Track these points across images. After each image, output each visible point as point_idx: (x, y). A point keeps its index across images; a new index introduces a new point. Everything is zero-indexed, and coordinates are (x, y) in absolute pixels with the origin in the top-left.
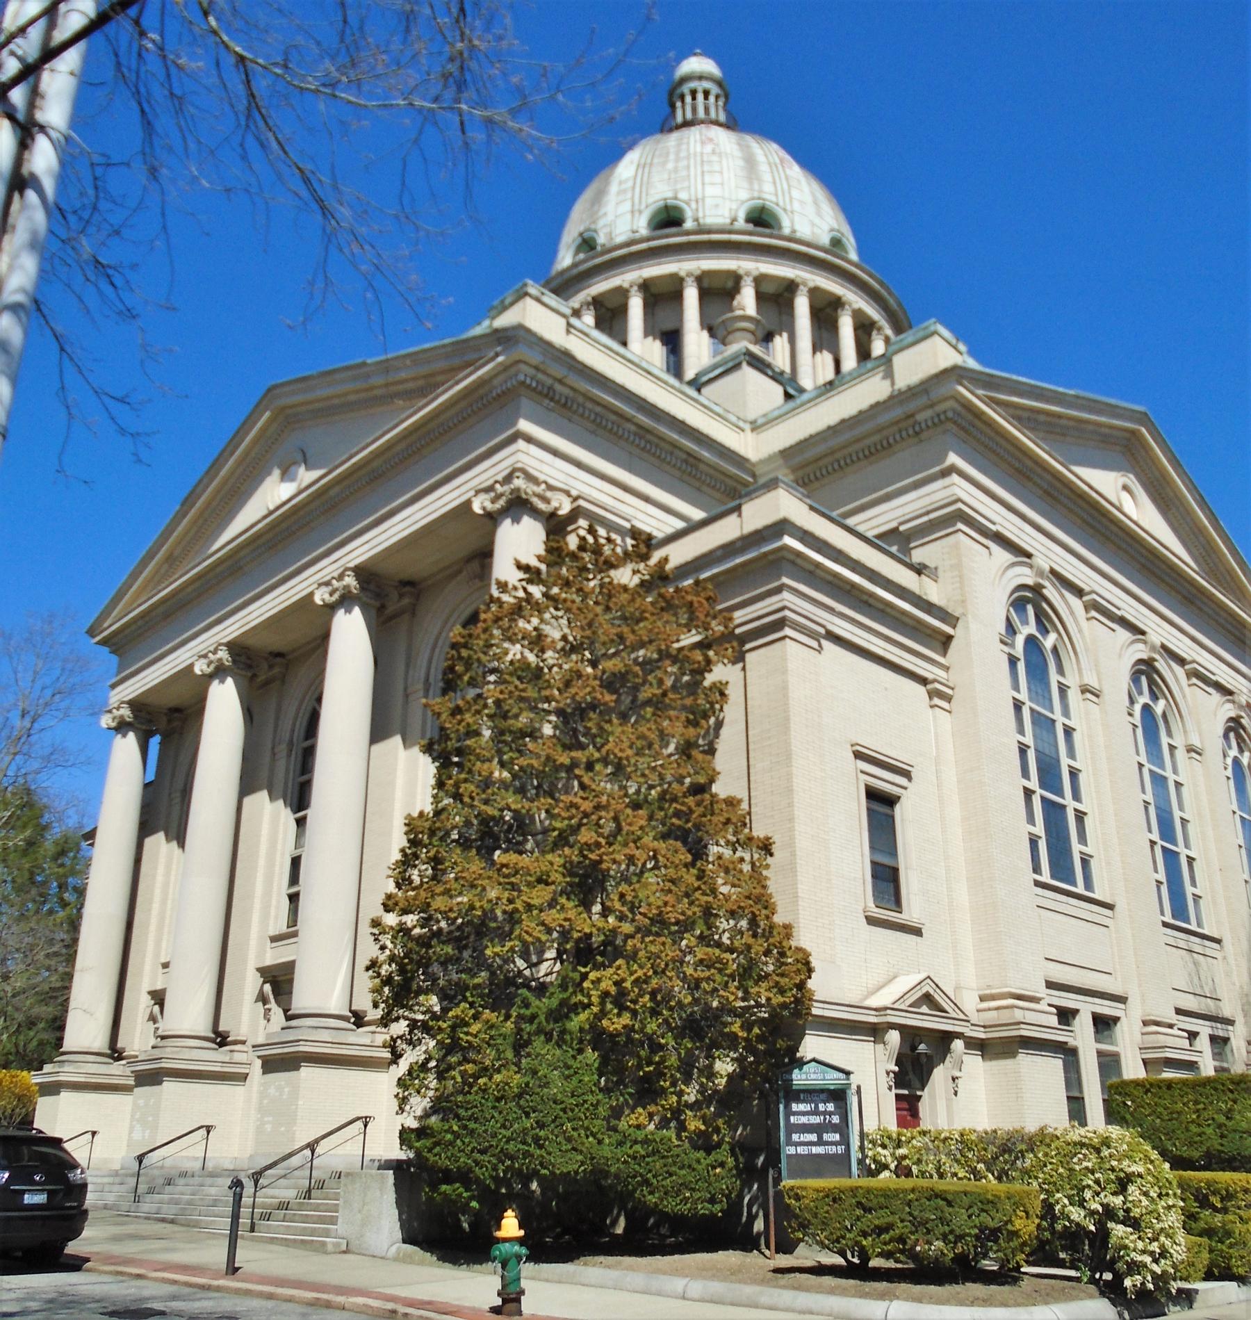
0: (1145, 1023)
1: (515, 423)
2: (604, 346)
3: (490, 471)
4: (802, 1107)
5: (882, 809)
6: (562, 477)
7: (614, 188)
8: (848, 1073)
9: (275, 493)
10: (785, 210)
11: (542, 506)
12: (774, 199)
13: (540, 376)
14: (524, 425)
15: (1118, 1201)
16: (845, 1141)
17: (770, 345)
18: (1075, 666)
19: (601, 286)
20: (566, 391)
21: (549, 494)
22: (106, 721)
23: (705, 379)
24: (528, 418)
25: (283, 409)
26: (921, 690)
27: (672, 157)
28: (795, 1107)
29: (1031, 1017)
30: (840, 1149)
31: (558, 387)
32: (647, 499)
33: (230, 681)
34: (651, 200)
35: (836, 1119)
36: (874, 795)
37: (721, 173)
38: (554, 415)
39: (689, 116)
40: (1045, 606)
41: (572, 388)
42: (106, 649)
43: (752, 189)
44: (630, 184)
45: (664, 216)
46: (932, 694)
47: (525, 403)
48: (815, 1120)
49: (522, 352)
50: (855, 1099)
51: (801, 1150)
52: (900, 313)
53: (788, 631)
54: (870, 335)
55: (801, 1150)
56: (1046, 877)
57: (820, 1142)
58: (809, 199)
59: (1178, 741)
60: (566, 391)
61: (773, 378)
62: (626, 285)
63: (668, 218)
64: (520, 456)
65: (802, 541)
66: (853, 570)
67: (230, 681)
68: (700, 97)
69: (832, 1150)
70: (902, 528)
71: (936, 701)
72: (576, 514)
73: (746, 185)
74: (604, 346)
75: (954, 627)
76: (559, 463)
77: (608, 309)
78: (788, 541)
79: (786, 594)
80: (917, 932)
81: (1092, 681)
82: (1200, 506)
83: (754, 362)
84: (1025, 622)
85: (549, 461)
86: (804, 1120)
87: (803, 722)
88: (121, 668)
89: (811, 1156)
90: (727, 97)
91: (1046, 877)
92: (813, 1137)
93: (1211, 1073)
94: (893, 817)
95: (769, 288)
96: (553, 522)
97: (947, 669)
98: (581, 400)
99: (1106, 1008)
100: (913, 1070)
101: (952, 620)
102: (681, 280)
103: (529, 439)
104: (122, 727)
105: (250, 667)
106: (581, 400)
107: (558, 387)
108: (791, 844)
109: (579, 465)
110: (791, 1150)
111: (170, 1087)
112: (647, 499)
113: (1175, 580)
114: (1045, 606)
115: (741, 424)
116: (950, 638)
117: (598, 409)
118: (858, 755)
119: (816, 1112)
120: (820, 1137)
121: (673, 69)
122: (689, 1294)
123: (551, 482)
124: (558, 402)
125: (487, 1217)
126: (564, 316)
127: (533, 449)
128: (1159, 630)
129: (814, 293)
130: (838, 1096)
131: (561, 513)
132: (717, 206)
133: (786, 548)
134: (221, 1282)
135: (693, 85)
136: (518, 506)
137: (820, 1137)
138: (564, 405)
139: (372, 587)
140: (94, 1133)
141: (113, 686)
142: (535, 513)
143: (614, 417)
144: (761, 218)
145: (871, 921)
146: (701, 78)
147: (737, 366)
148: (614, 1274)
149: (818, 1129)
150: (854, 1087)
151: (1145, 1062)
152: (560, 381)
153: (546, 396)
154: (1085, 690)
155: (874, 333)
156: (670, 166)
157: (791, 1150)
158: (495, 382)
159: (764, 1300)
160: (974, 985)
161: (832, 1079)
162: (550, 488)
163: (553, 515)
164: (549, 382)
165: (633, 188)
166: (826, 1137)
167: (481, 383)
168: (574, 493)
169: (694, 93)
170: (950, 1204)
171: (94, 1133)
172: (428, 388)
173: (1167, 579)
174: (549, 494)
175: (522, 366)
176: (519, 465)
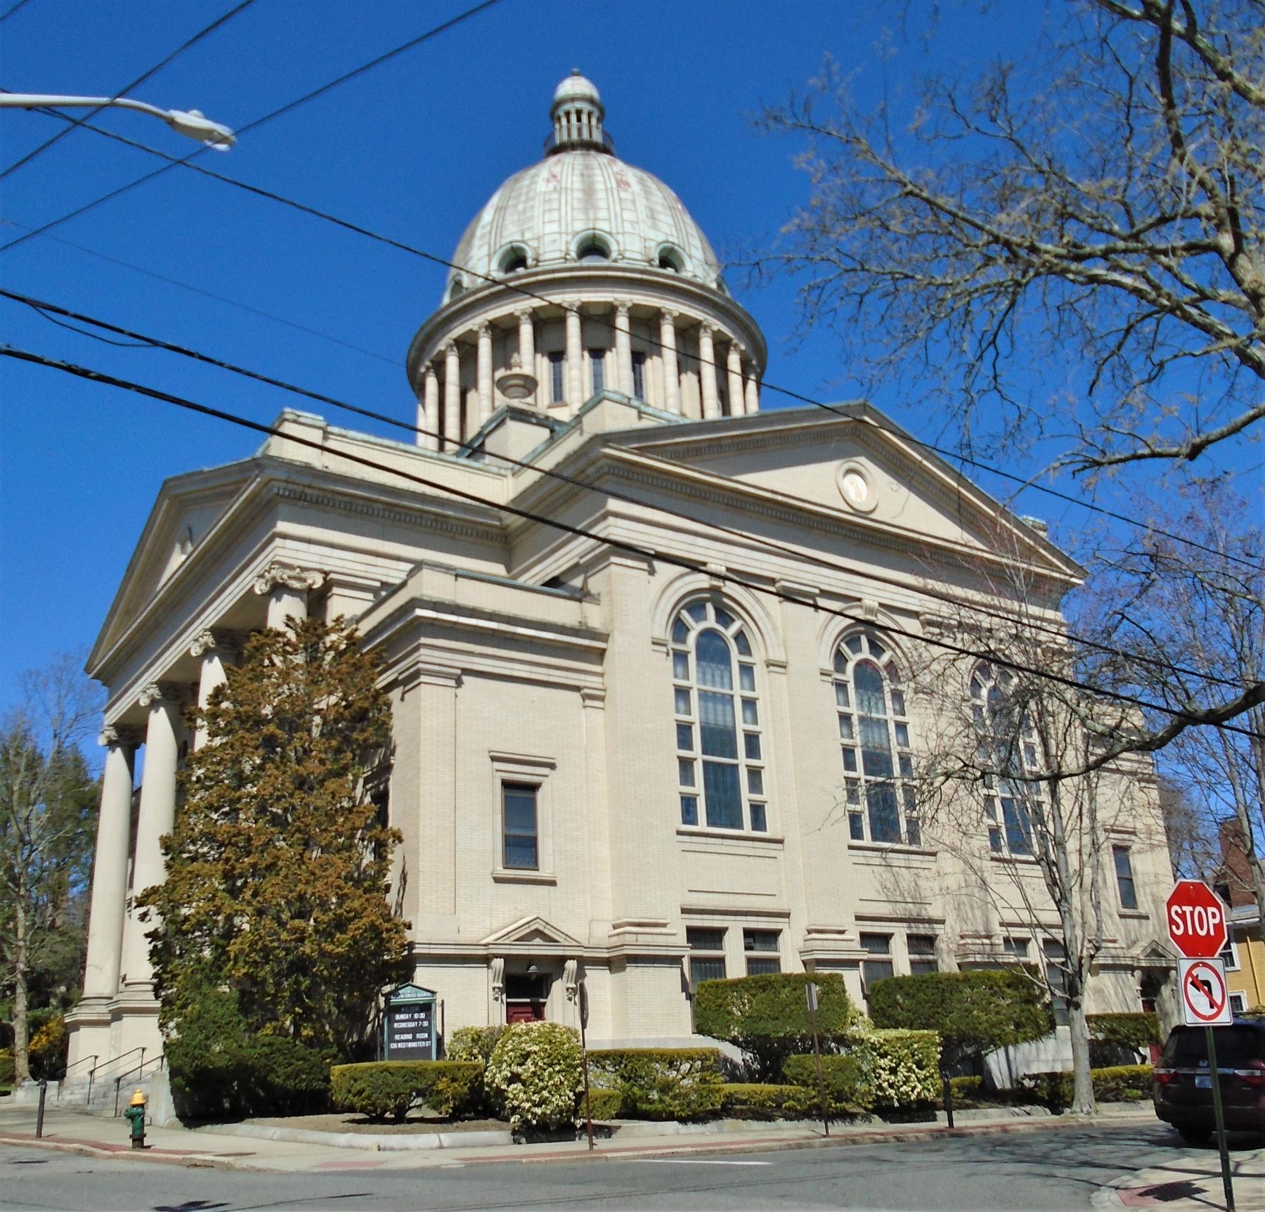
0: (809, 932)
1: (274, 526)
3: (261, 564)
4: (403, 1017)
6: (316, 558)
7: (479, 233)
8: (433, 993)
9: (177, 560)
10: (610, 234)
11: (296, 585)
13: (290, 486)
14: (282, 526)
15: (520, 1070)
17: (603, 360)
18: (762, 645)
19: (458, 330)
20: (315, 492)
21: (304, 575)
22: (102, 741)
23: (486, 431)
24: (284, 520)
25: (177, 496)
26: (576, 696)
27: (523, 198)
28: (398, 1017)
30: (428, 1044)
31: (307, 491)
33: (162, 710)
34: (504, 242)
35: (426, 1024)
37: (559, 210)
40: (726, 600)
41: (320, 489)
42: (99, 682)
44: (488, 228)
45: (513, 256)
46: (586, 697)
47: (283, 508)
48: (412, 1025)
49: (270, 473)
50: (439, 1009)
51: (400, 1045)
52: (728, 305)
53: (423, 678)
54: (698, 332)
55: (400, 1045)
57: (414, 1040)
58: (643, 213)
60: (315, 492)
61: (538, 424)
62: (475, 328)
63: (515, 259)
64: (278, 551)
65: (433, 609)
66: (490, 620)
67: (162, 710)
68: (574, 118)
69: (422, 1044)
70: (582, 561)
71: (588, 702)
72: (328, 585)
73: (582, 216)
75: (606, 641)
77: (503, 330)
78: (419, 612)
79: (422, 651)
80: (552, 883)
81: (777, 655)
82: (942, 470)
83: (518, 416)
85: (301, 547)
86: (403, 1025)
87: (447, 737)
88: (110, 696)
92: (410, 1036)
97: (602, 675)
98: (330, 495)
101: (604, 637)
102: (518, 318)
103: (285, 536)
104: (111, 744)
105: (177, 697)
106: (330, 495)
107: (307, 491)
108: (417, 836)
110: (394, 1046)
111: (128, 1020)
114: (726, 600)
115: (503, 472)
116: (604, 650)
117: (346, 499)
119: (412, 1020)
120: (414, 1037)
121: (554, 88)
122: (445, 1144)
124: (311, 501)
126: (320, 428)
127: (289, 543)
130: (426, 1007)
131: (315, 587)
132: (554, 241)
133: (419, 617)
134: (34, 1142)
135: (567, 107)
136: (278, 589)
138: (317, 502)
139: (227, 639)
140: (144, 1049)
141: (106, 711)
142: (293, 592)
143: (361, 502)
144: (593, 247)
146: (573, 99)
147: (502, 423)
148: (297, 1133)
149: (413, 1031)
150: (439, 1001)
151: (805, 963)
152: (309, 487)
153: (300, 499)
154: (769, 664)
155: (702, 331)
156: (520, 207)
157: (394, 1046)
158: (264, 493)
159: (301, 1138)
160: (610, 918)
161: (422, 997)
162: (303, 569)
164: (300, 489)
165: (490, 232)
166: (418, 1036)
167: (254, 495)
169: (568, 114)
170: (392, 1074)
171: (144, 1049)
172: (233, 494)
174: (304, 575)
176: (277, 558)
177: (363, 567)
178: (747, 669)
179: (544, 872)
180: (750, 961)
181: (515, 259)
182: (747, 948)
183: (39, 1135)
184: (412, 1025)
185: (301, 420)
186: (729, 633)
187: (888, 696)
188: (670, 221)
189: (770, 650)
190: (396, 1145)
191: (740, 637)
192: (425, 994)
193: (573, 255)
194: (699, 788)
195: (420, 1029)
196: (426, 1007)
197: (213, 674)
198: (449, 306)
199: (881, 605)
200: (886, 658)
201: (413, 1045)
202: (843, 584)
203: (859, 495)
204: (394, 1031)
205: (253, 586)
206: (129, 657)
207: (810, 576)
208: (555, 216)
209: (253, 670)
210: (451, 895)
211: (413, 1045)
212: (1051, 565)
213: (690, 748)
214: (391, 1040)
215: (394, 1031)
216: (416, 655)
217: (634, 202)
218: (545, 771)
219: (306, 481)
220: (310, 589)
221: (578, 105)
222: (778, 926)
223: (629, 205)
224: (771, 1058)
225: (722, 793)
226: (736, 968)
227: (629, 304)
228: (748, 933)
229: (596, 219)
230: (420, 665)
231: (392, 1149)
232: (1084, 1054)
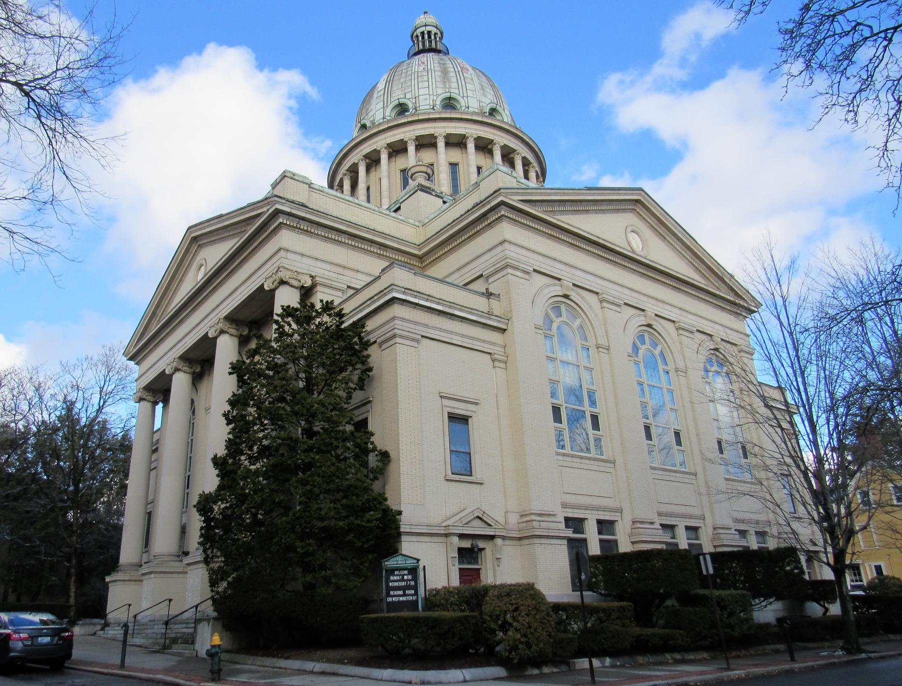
5: (459, 426)
8: (418, 560)
12: (457, 91)
16: (416, 594)
19: (366, 148)
29: (554, 525)
30: (414, 598)
35: (413, 583)
39: (421, 47)
43: (445, 88)
48: (403, 584)
57: (404, 595)
58: (478, 87)
59: (671, 367)
61: (436, 196)
63: (402, 109)
73: (441, 86)
86: (396, 584)
89: (399, 602)
91: (568, 450)
92: (401, 592)
93: (687, 547)
102: (406, 142)
110: (390, 599)
120: (404, 592)
122: (468, 678)
123: (298, 270)
137: (404, 592)
144: (449, 103)
150: (421, 567)
156: (402, 80)
157: (390, 599)
161: (410, 563)
180: (601, 541)
183: (122, 666)
184: (403, 584)
187: (661, 372)
188: (492, 93)
189: (599, 338)
190: (433, 680)
192: (412, 561)
193: (438, 107)
195: (408, 587)
196: (413, 571)
197: (227, 350)
198: (356, 137)
200: (659, 348)
201: (404, 599)
204: (389, 589)
205: (263, 285)
206: (274, 216)
207: (617, 294)
208: (426, 84)
209: (99, 471)
211: (404, 599)
213: (557, 398)
214: (388, 595)
215: (389, 589)
216: (392, 324)
217: (472, 79)
220: (303, 287)
221: (429, 28)
223: (469, 81)
227: (475, 136)
228: (600, 522)
229: (450, 88)
230: (396, 331)
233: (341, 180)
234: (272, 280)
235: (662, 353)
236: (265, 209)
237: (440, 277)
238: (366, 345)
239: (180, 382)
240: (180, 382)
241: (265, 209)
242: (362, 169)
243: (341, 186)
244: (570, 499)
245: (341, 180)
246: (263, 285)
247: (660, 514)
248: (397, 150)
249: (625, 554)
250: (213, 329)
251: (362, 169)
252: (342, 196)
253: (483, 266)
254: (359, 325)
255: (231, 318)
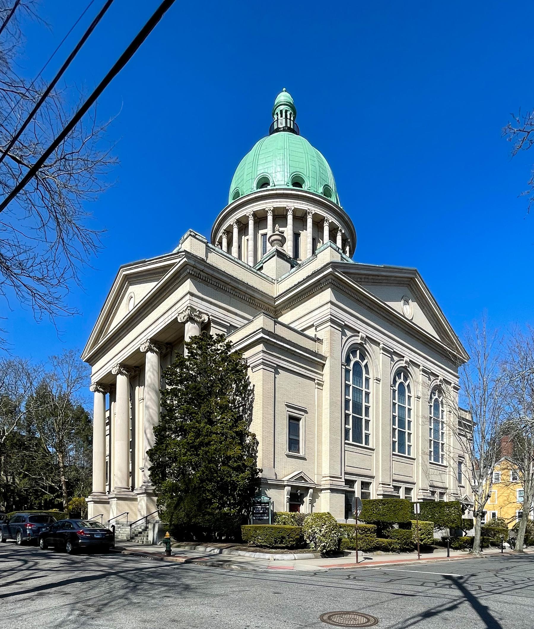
2: (221, 254)
8: (270, 498)
13: (195, 269)
22: (92, 388)
32: (236, 314)
36: (291, 418)
38: (201, 284)
56: (351, 441)
63: (264, 183)
74: (221, 254)
76: (204, 303)
80: (304, 459)
84: (355, 356)
90: (295, 113)
94: (298, 425)
95: (299, 214)
96: (203, 325)
99: (366, 480)
100: (295, 499)
106: (210, 278)
109: (211, 303)
112: (236, 314)
113: (420, 336)
115: (273, 281)
116: (324, 364)
117: (217, 281)
118: (288, 406)
125: (172, 539)
126: (204, 242)
128: (410, 356)
129: (315, 215)
140: (128, 513)
145: (288, 456)
163: (203, 322)
168: (210, 314)
171: (128, 513)
173: (416, 336)
175: (188, 266)
177: (223, 316)
178: (367, 379)
179: (301, 454)
181: (264, 183)
182: (362, 489)
185: (197, 236)
186: (363, 364)
191: (366, 366)
194: (350, 426)
199: (410, 361)
202: (400, 350)
203: (407, 312)
205: (177, 318)
210: (272, 461)
212: (459, 352)
218: (303, 413)
219: (202, 267)
222: (371, 481)
224: (381, 529)
225: (355, 431)
226: (358, 495)
231: (278, 560)
232: (479, 533)
233: (221, 237)
234: (183, 315)
235: (408, 386)
236: (178, 260)
237: (286, 323)
238: (246, 367)
239: (122, 382)
240: (122, 382)
241: (178, 260)
242: (235, 231)
243: (220, 243)
244: (349, 470)
245: (221, 237)
246: (177, 318)
247: (394, 481)
248: (260, 219)
249: (375, 501)
250: (143, 346)
251: (235, 231)
252: (220, 251)
253: (314, 318)
254: (239, 353)
255: (154, 341)
